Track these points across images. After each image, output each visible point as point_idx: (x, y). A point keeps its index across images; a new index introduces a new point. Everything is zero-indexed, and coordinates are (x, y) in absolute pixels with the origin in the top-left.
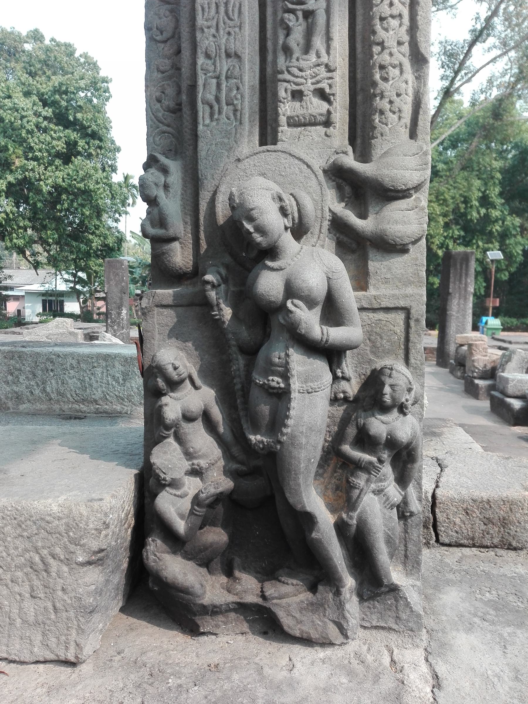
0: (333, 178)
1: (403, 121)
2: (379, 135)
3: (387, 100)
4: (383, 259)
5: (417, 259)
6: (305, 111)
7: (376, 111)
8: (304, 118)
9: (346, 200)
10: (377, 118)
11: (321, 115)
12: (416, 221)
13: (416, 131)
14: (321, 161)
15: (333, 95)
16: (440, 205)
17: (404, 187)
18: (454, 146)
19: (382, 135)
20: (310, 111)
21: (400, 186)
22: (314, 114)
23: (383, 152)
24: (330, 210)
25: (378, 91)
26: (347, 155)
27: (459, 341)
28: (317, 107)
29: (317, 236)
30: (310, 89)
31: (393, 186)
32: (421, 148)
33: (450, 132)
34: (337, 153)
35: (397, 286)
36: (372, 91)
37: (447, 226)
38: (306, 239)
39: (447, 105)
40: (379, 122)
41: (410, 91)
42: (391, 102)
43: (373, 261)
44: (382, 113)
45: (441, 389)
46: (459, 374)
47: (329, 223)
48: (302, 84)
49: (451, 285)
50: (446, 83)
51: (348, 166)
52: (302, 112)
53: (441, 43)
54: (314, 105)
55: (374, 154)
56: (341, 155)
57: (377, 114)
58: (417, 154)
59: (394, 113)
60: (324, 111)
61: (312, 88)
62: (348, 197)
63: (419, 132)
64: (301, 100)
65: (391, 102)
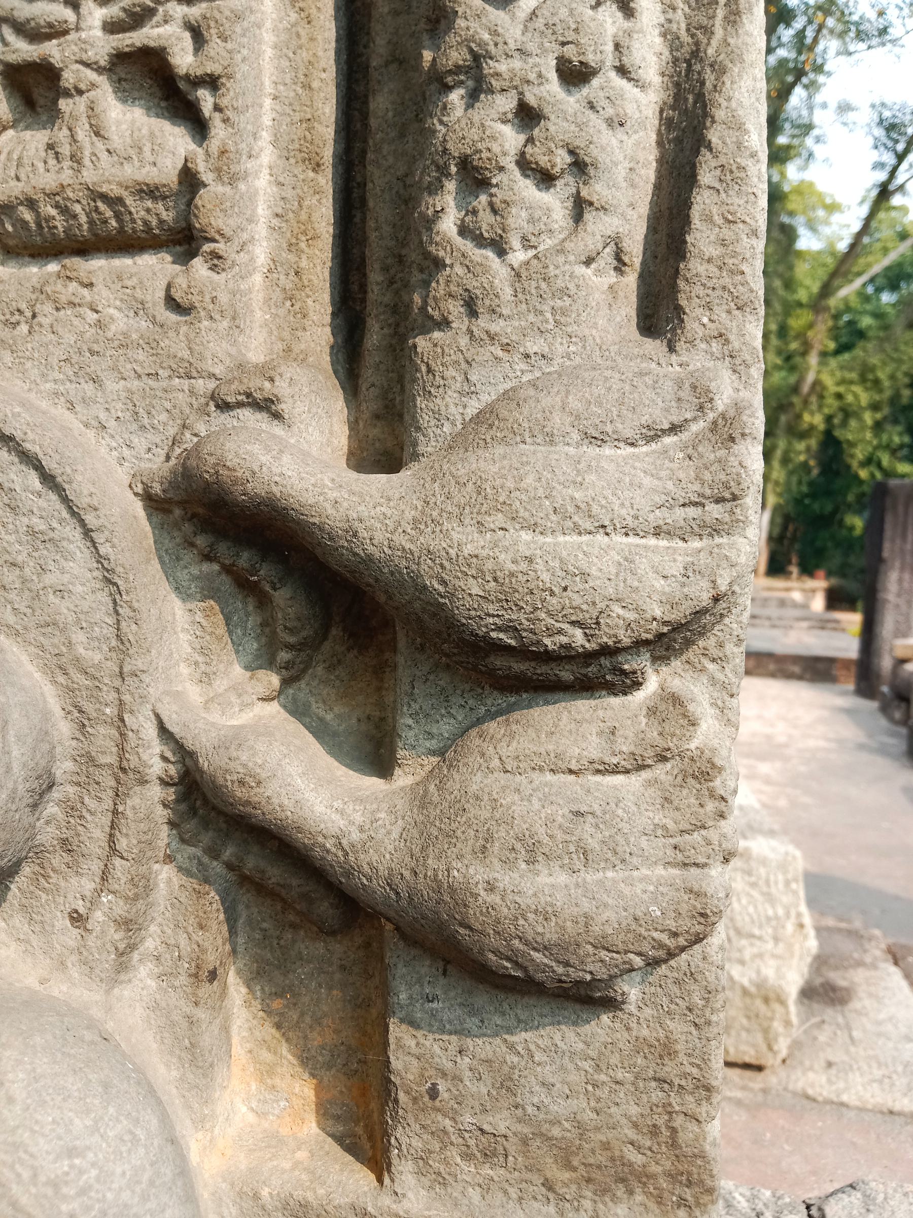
0: (201, 541)
1: (598, 226)
2: (455, 309)
3: (506, 103)
4: (471, 1023)
5: (667, 1050)
6: (67, 176)
7: (443, 171)
8: (64, 211)
9: (284, 656)
10: (448, 213)
11: (150, 192)
12: (659, 847)
13: (674, 289)
14: (140, 442)
15: (212, 82)
16: (867, 389)
17: (578, 637)
18: (894, 286)
19: (471, 308)
20: (89, 176)
21: (551, 632)
22: (114, 190)
23: (474, 407)
24: (164, 732)
25: (457, 56)
26: (277, 416)
27: (900, 653)
28: (132, 144)
29: (96, 866)
30: (91, 55)
31: (511, 628)
32: (703, 398)
33: (886, 261)
34: (224, 406)
35: (548, 1185)
36: (428, 55)
37: (878, 426)
38: (35, 879)
39: (882, 215)
40: (463, 231)
41: (650, 55)
42: (527, 116)
43: (413, 1023)
44: (475, 177)
45: (861, 747)
46: (898, 715)
47: (171, 794)
48: (56, 31)
49: (887, 547)
50: (882, 176)
51: (257, 488)
52: (49, 181)
53: (873, 106)
54: (116, 142)
55: (425, 419)
56: (246, 414)
57: (451, 186)
58: (674, 429)
59: (546, 179)
60: (166, 172)
61: (102, 46)
62: (289, 647)
63: (691, 298)
64: (53, 116)
65: (527, 116)
